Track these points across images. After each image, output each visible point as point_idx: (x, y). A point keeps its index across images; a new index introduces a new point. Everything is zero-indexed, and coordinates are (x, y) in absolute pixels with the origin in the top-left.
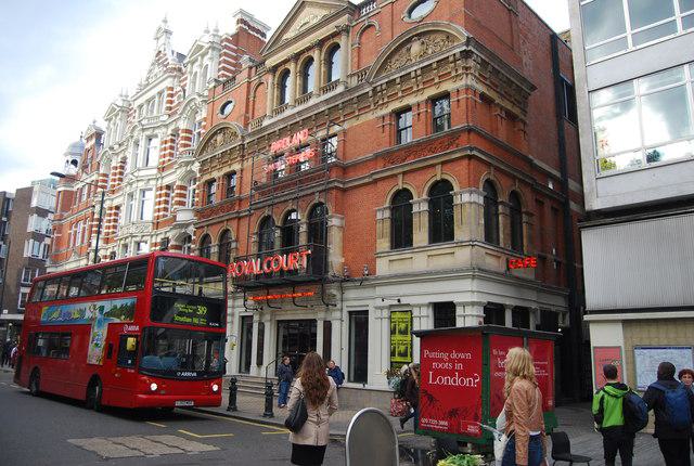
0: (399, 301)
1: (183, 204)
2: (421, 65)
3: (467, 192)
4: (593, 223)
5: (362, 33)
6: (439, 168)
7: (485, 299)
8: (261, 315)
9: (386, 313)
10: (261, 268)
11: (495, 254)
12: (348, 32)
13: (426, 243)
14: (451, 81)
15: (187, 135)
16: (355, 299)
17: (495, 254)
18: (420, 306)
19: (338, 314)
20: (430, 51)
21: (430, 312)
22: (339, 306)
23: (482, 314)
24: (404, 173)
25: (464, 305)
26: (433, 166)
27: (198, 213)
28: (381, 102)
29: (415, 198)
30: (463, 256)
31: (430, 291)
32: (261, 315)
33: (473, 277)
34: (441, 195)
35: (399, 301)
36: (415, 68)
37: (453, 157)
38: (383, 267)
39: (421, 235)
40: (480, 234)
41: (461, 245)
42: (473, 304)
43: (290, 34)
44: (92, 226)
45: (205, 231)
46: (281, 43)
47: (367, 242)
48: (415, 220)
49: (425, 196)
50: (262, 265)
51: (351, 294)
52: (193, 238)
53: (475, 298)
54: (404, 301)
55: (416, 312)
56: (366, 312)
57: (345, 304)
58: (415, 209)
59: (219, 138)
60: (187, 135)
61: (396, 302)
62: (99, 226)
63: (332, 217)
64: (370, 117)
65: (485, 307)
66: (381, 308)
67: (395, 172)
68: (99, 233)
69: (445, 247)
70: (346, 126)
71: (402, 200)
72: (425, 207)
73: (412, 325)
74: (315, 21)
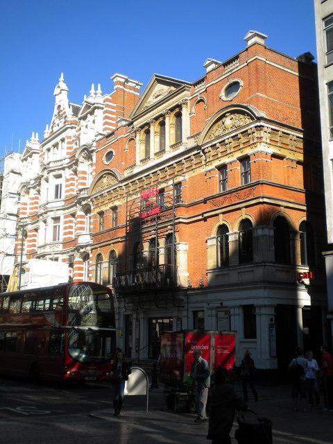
0: (221, 304)
1: (82, 229)
3: (261, 228)
4: (292, 256)
7: (275, 302)
8: (138, 314)
9: (214, 312)
10: (133, 281)
11: (285, 269)
13: (237, 263)
14: (249, 147)
15: (84, 175)
17: (285, 269)
18: (234, 307)
19: (185, 313)
21: (240, 311)
22: (186, 308)
23: (273, 313)
25: (260, 307)
26: (97, 248)
27: (93, 236)
28: (251, 142)
29: (230, 232)
30: (259, 273)
32: (138, 314)
33: (265, 288)
35: (221, 304)
40: (271, 256)
41: (258, 265)
42: (265, 306)
44: (16, 245)
45: (99, 251)
50: (133, 278)
52: (91, 256)
53: (266, 302)
54: (225, 304)
55: (232, 311)
60: (84, 175)
61: (219, 305)
62: (23, 245)
63: (179, 244)
64: (203, 170)
65: (275, 309)
66: (212, 309)
68: (22, 250)
69: (248, 267)
73: (181, 326)
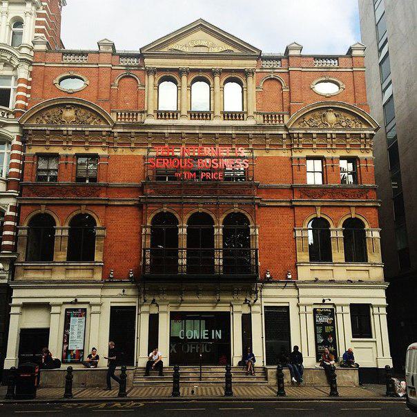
2: (337, 132)
5: (124, 77)
6: (319, 210)
12: (253, 74)
16: (272, 296)
18: (342, 306)
20: (344, 124)
24: (323, 207)
31: (365, 295)
34: (354, 231)
36: (331, 132)
37: (116, 203)
38: (304, 273)
39: (338, 254)
41: (374, 265)
43: (179, 46)
46: (165, 50)
47: (284, 252)
48: (333, 243)
49: (340, 227)
51: (266, 292)
55: (339, 309)
56: (288, 308)
57: (264, 300)
58: (333, 234)
59: (69, 114)
64: (142, 152)
67: (351, 204)
69: (361, 266)
70: (256, 154)
71: (321, 228)
72: (341, 235)
74: (216, 50)
